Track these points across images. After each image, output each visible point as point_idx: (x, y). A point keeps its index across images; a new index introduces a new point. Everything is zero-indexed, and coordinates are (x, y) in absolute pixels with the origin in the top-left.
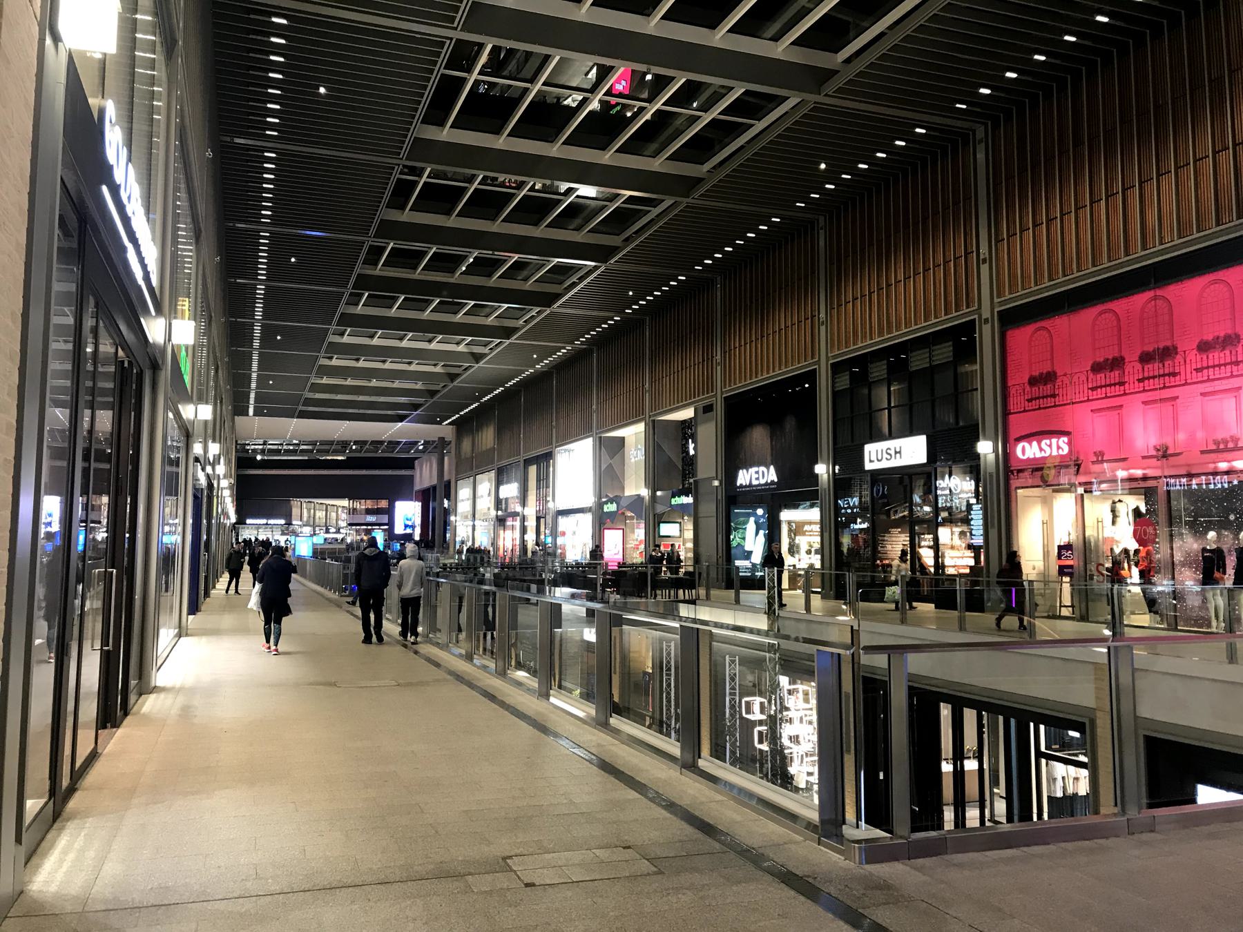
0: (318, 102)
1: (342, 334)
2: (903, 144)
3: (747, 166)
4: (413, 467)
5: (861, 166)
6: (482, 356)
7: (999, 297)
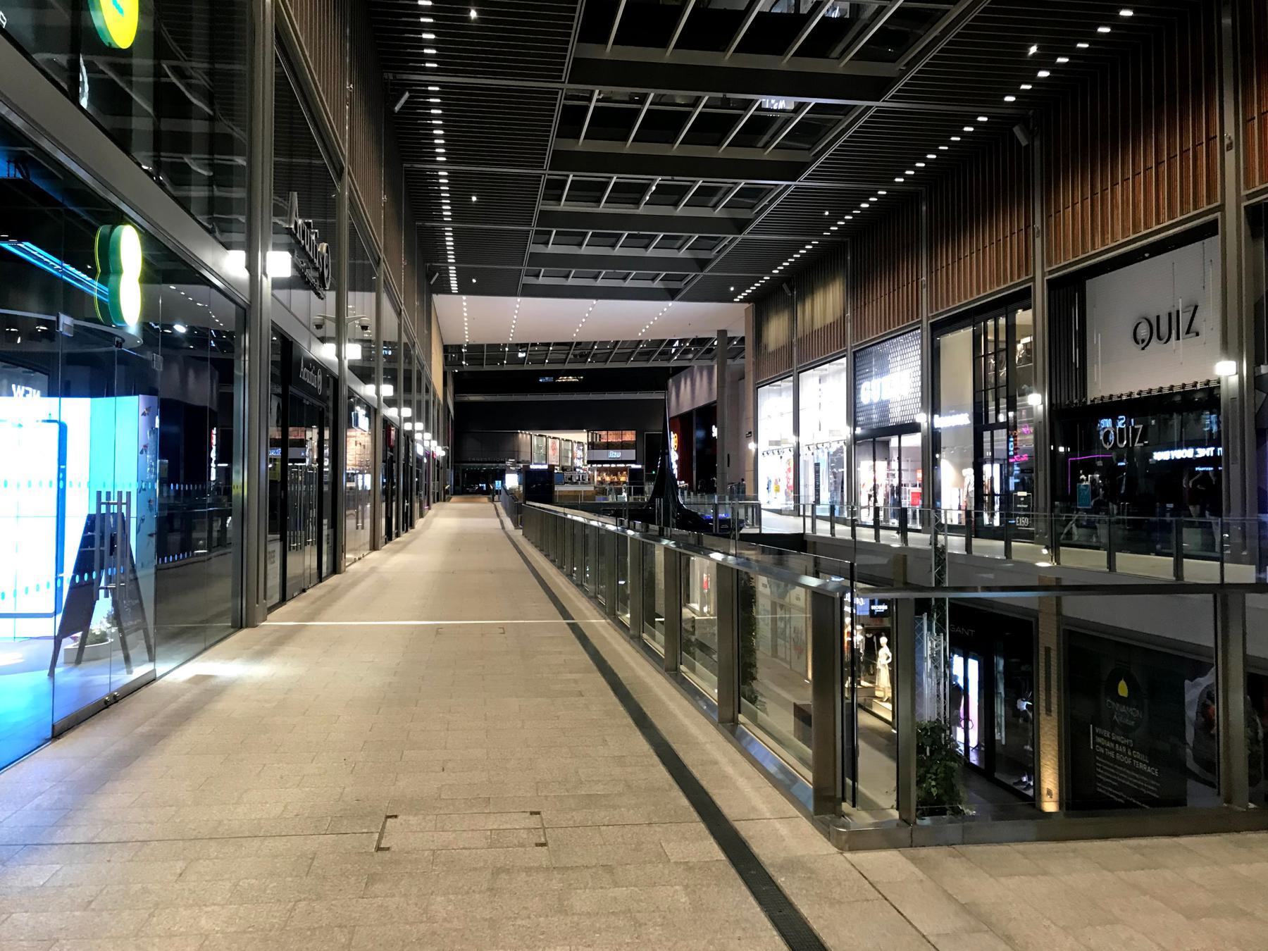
0: (471, 28)
1: (537, 276)
2: (1086, 46)
3: (915, 85)
4: (664, 387)
5: (1060, 60)
6: (708, 261)
7: (1247, 188)
